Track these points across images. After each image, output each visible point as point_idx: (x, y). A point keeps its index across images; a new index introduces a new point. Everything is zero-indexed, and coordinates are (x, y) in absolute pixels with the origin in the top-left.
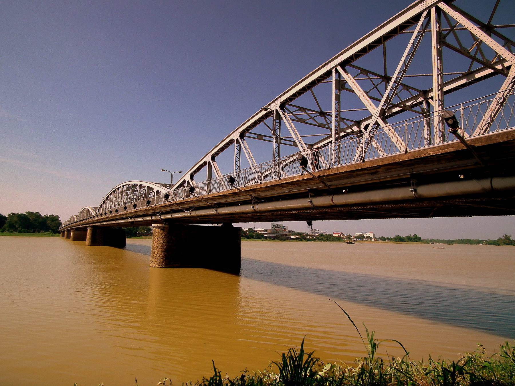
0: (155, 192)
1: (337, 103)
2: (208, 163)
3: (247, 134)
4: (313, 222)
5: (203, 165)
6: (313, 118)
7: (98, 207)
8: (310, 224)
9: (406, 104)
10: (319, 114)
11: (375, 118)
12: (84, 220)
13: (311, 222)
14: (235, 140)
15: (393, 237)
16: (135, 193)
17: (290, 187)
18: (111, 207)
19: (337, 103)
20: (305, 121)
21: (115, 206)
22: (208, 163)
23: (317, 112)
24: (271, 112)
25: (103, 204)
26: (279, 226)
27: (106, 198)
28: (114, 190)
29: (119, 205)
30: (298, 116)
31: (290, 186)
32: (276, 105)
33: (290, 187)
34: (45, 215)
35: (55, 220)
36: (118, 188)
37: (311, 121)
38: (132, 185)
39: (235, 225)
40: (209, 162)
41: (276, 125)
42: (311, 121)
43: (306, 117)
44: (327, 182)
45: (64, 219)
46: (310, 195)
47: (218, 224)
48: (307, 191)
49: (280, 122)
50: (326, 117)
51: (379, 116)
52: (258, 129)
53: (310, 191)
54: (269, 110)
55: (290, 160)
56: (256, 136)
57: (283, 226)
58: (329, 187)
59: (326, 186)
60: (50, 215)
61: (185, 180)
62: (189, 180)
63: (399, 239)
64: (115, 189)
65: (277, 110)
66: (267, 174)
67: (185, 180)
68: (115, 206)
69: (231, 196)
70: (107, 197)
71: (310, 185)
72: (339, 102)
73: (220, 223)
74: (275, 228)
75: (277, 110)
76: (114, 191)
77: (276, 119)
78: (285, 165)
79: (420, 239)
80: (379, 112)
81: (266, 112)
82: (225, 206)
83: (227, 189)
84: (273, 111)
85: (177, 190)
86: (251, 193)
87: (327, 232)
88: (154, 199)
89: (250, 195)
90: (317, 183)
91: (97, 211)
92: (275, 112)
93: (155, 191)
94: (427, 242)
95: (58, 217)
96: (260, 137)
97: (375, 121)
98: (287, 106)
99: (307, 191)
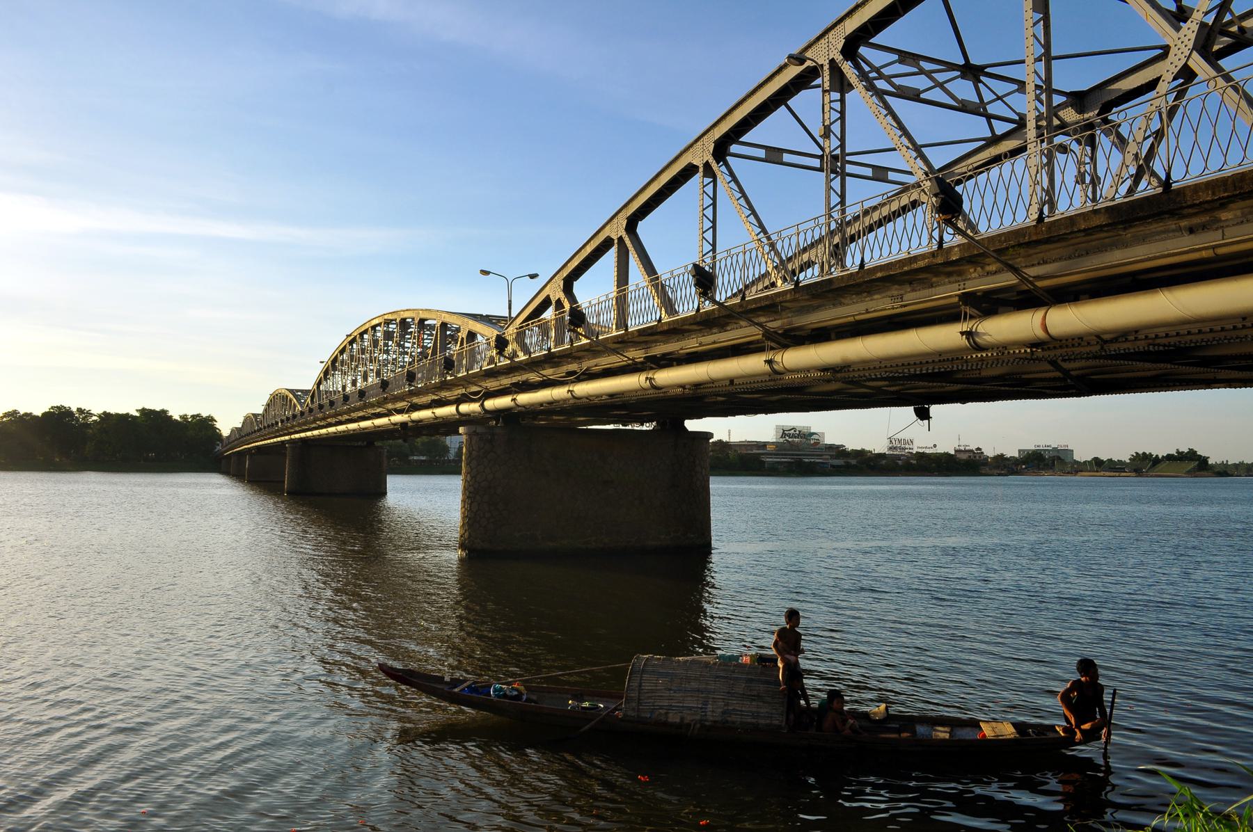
0: (463, 339)
1: (1038, 21)
2: (616, 241)
3: (734, 148)
4: (935, 410)
5: (639, 217)
6: (941, 85)
7: (310, 391)
8: (923, 415)
9: (1230, 29)
10: (959, 73)
11: (1180, 56)
12: (277, 423)
13: (928, 409)
14: (613, 240)
15: (1123, 454)
16: (407, 345)
17: (895, 293)
18: (344, 387)
19: (1038, 21)
20: (919, 95)
21: (354, 383)
22: (616, 241)
23: (951, 66)
24: (814, 72)
25: (330, 368)
26: (800, 432)
27: (330, 363)
28: (350, 338)
29: (365, 378)
30: (897, 81)
31: (896, 289)
32: (831, 46)
33: (895, 293)
34: (181, 417)
35: (204, 426)
36: (362, 334)
37: (937, 95)
38: (398, 321)
39: (692, 425)
40: (621, 239)
41: (831, 108)
42: (937, 95)
43: (920, 82)
44: (1026, 267)
45: (226, 425)
46: (966, 313)
47: (642, 425)
48: (956, 299)
49: (842, 101)
50: (981, 82)
51: (1193, 49)
52: (765, 133)
53: (967, 298)
54: (808, 63)
55: (878, 212)
56: (761, 153)
57: (812, 431)
58: (1031, 283)
59: (1024, 279)
60: (193, 416)
61: (548, 297)
62: (562, 295)
63: (1144, 465)
64: (352, 337)
65: (832, 62)
66: (893, 210)
67: (548, 297)
68: (354, 383)
69: (696, 330)
70: (332, 359)
71: (964, 280)
72: (1046, 20)
73: (650, 421)
74: (787, 438)
75: (832, 62)
76: (351, 343)
77: (832, 89)
78: (880, 220)
79: (1203, 462)
80: (1195, 33)
81: (800, 69)
82: (675, 363)
83: (688, 303)
84: (822, 65)
85: (528, 325)
86: (762, 319)
87: (935, 446)
88: (460, 355)
89: (760, 325)
90: (988, 273)
91: (309, 399)
92: (826, 67)
93: (463, 334)
94: (1224, 471)
95: (213, 420)
96: (774, 155)
97: (1180, 64)
98: (863, 50)
99: (956, 299)
